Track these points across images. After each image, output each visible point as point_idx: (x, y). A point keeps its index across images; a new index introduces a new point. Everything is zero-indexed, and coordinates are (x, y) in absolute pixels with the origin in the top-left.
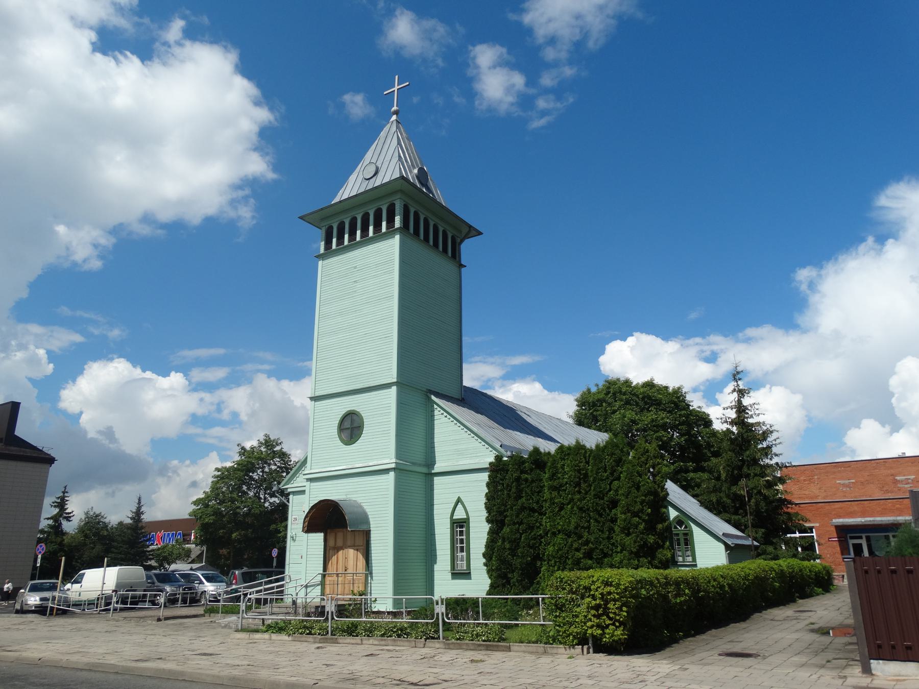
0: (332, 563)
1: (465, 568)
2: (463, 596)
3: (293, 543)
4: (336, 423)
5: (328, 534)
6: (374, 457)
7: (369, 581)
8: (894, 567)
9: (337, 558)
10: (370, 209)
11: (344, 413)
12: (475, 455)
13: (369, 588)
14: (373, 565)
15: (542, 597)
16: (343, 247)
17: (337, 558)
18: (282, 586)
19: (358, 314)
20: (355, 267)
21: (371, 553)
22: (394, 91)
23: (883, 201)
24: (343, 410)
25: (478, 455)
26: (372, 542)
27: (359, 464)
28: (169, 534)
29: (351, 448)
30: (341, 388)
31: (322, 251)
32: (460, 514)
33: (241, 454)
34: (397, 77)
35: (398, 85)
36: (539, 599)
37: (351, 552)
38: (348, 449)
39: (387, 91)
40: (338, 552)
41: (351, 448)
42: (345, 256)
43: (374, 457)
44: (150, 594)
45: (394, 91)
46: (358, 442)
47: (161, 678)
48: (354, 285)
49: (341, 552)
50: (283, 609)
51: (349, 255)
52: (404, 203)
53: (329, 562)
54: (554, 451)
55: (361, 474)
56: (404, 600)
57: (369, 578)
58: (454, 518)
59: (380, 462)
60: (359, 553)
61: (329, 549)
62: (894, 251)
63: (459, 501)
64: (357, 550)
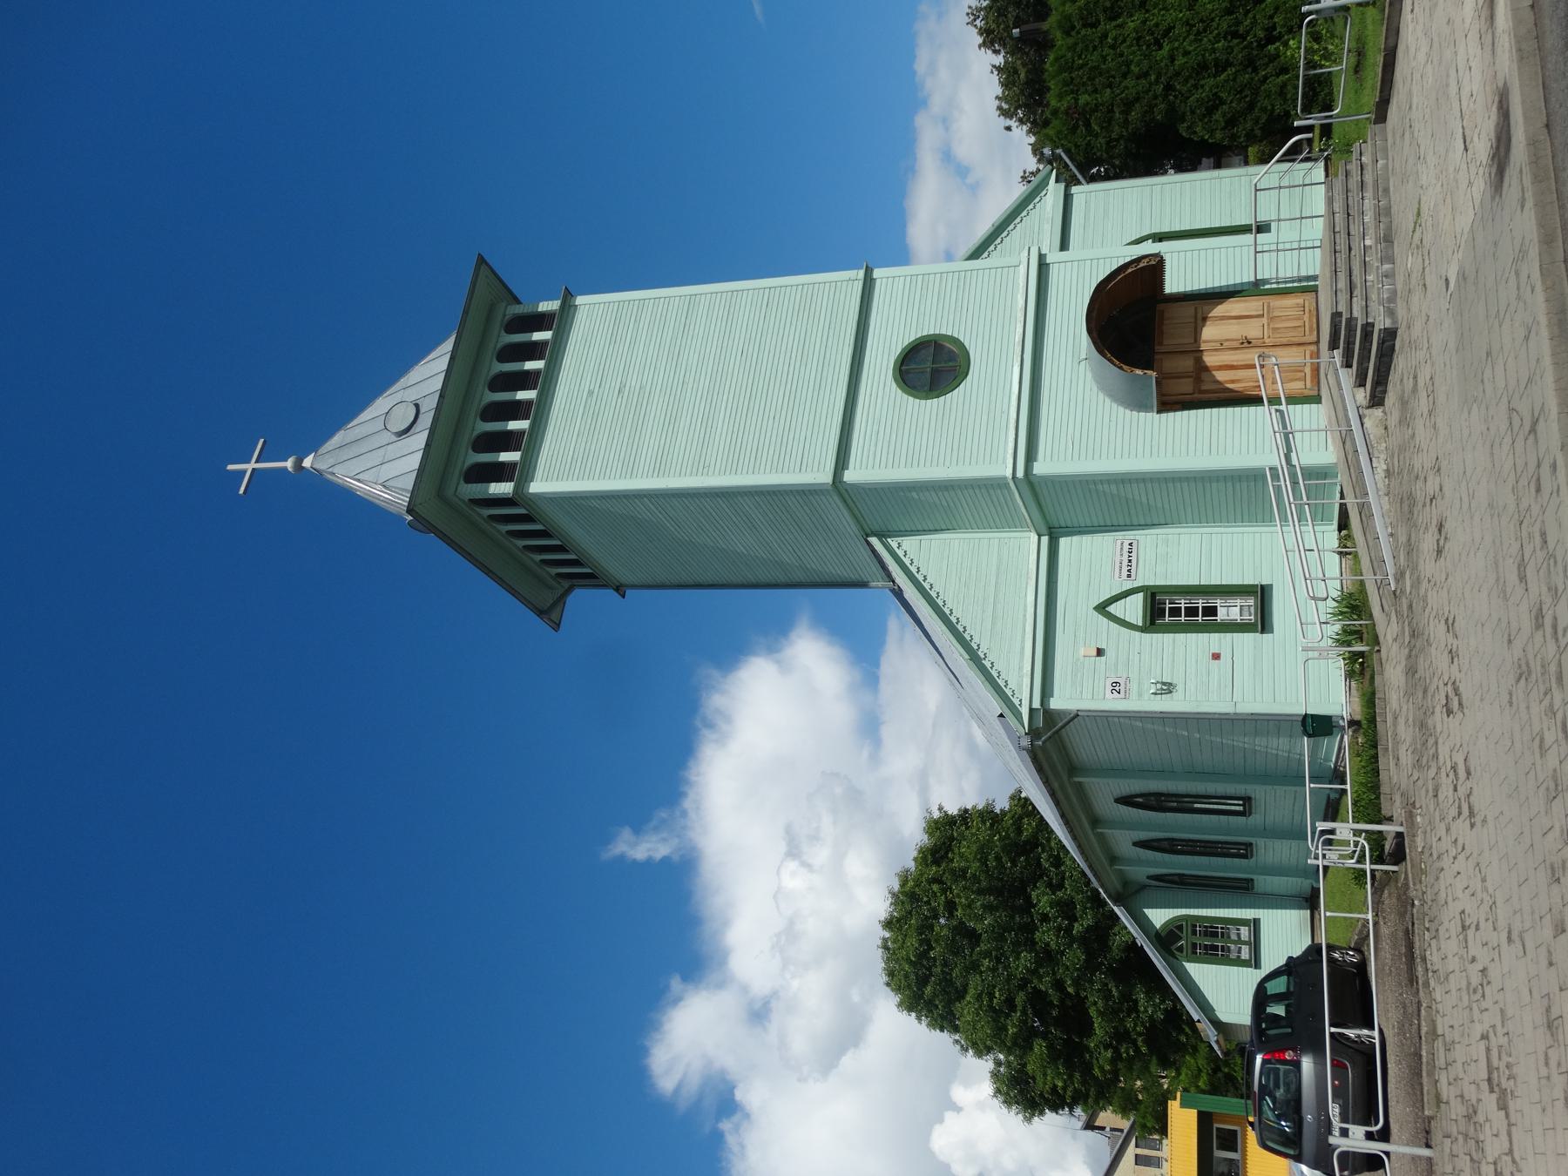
0: (1233, 382)
1: (1251, 602)
3: (1178, 694)
6: (1009, 303)
7: (1274, 286)
9: (1220, 368)
11: (894, 385)
12: (1036, 235)
13: (1288, 285)
14: (1238, 281)
15: (1309, 783)
16: (546, 377)
17: (1220, 368)
18: (1284, 519)
19: (692, 380)
20: (591, 393)
21: (1213, 288)
23: (666, 1083)
24: (888, 383)
25: (1036, 229)
26: (1189, 289)
29: (978, 361)
32: (1133, 609)
33: (981, 34)
34: (230, 467)
35: (244, 472)
36: (1313, 788)
37: (1209, 332)
38: (977, 371)
39: (240, 486)
40: (1206, 369)
41: (978, 361)
42: (552, 429)
43: (1009, 303)
44: (1332, 1025)
47: (1545, 96)
49: (1210, 360)
50: (1338, 261)
51: (554, 417)
53: (1231, 391)
55: (1042, 292)
56: (1328, 914)
57: (1267, 287)
58: (1140, 624)
60: (1210, 315)
61: (1201, 392)
62: (752, 1095)
63: (1102, 608)
64: (1205, 319)
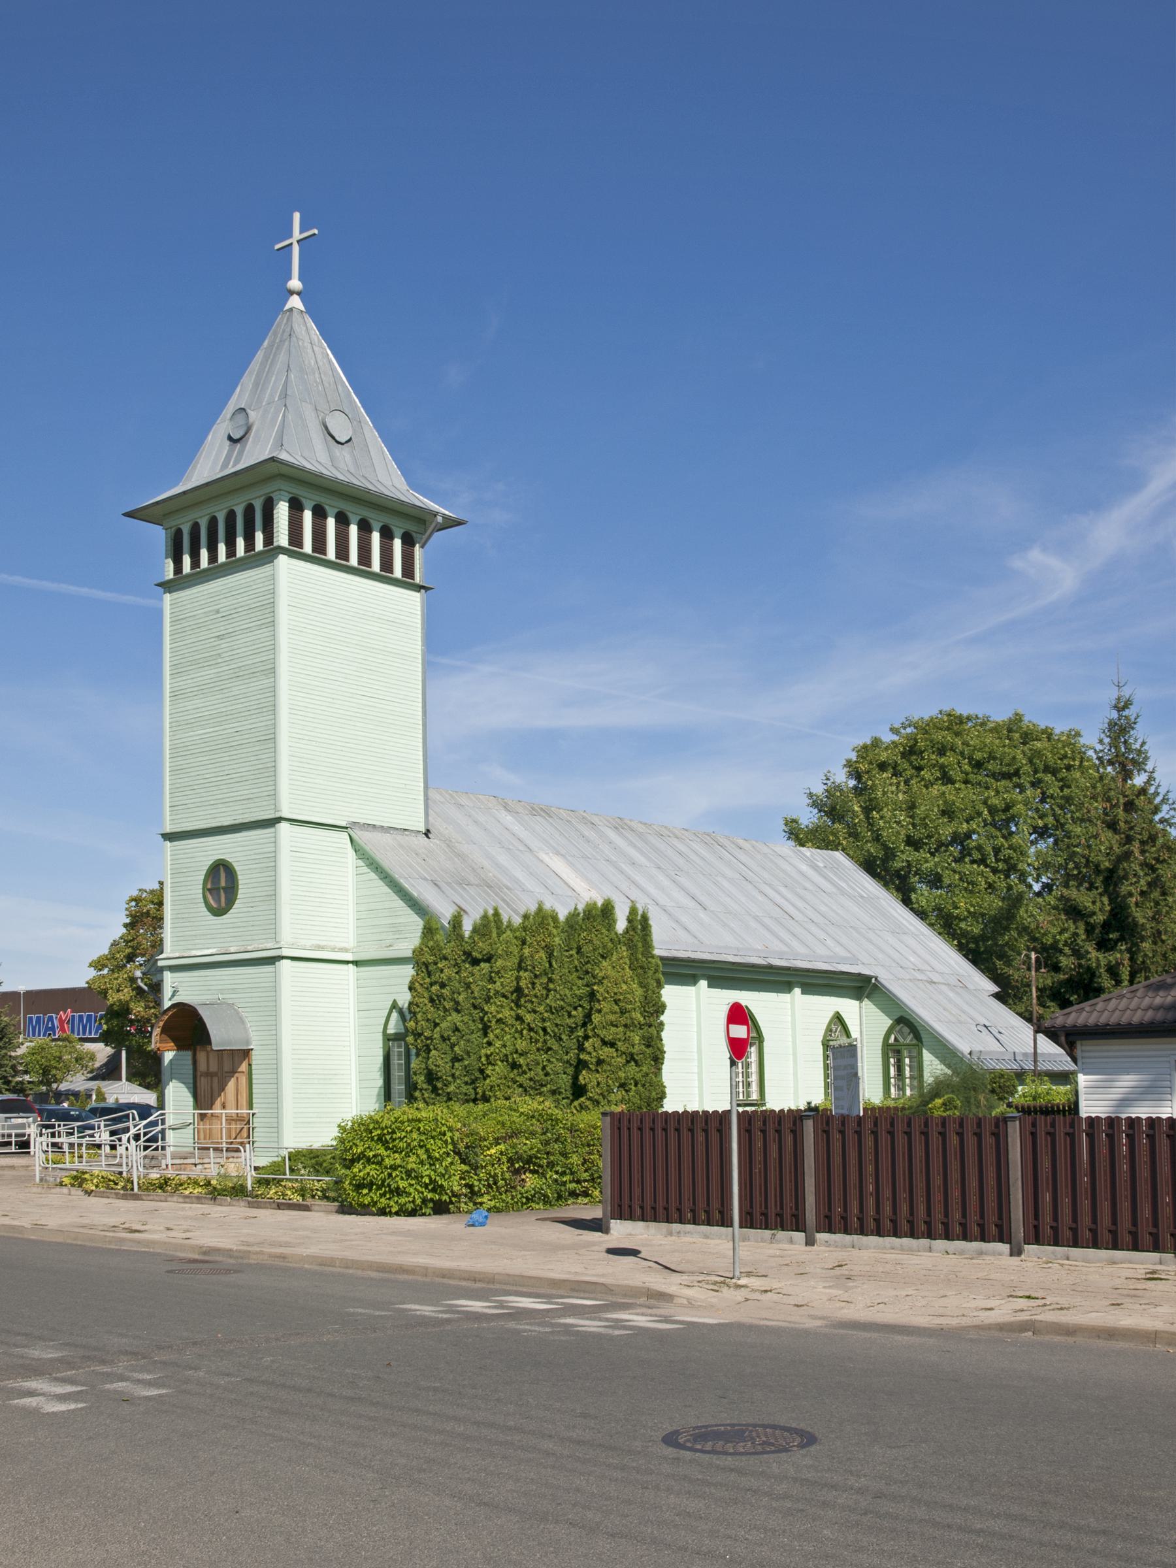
2: (91, 1232)
4: (238, 868)
5: (198, 1053)
8: (108, 1391)
10: (256, 498)
11: (211, 862)
16: (234, 561)
20: (218, 612)
22: (291, 244)
24: (210, 858)
27: (235, 948)
28: (81, 1017)
29: (221, 922)
30: (205, 821)
31: (170, 575)
34: (297, 216)
35: (301, 232)
41: (221, 922)
45: (291, 244)
46: (231, 911)
48: (215, 643)
52: (291, 496)
54: (109, 1048)
59: (261, 946)
